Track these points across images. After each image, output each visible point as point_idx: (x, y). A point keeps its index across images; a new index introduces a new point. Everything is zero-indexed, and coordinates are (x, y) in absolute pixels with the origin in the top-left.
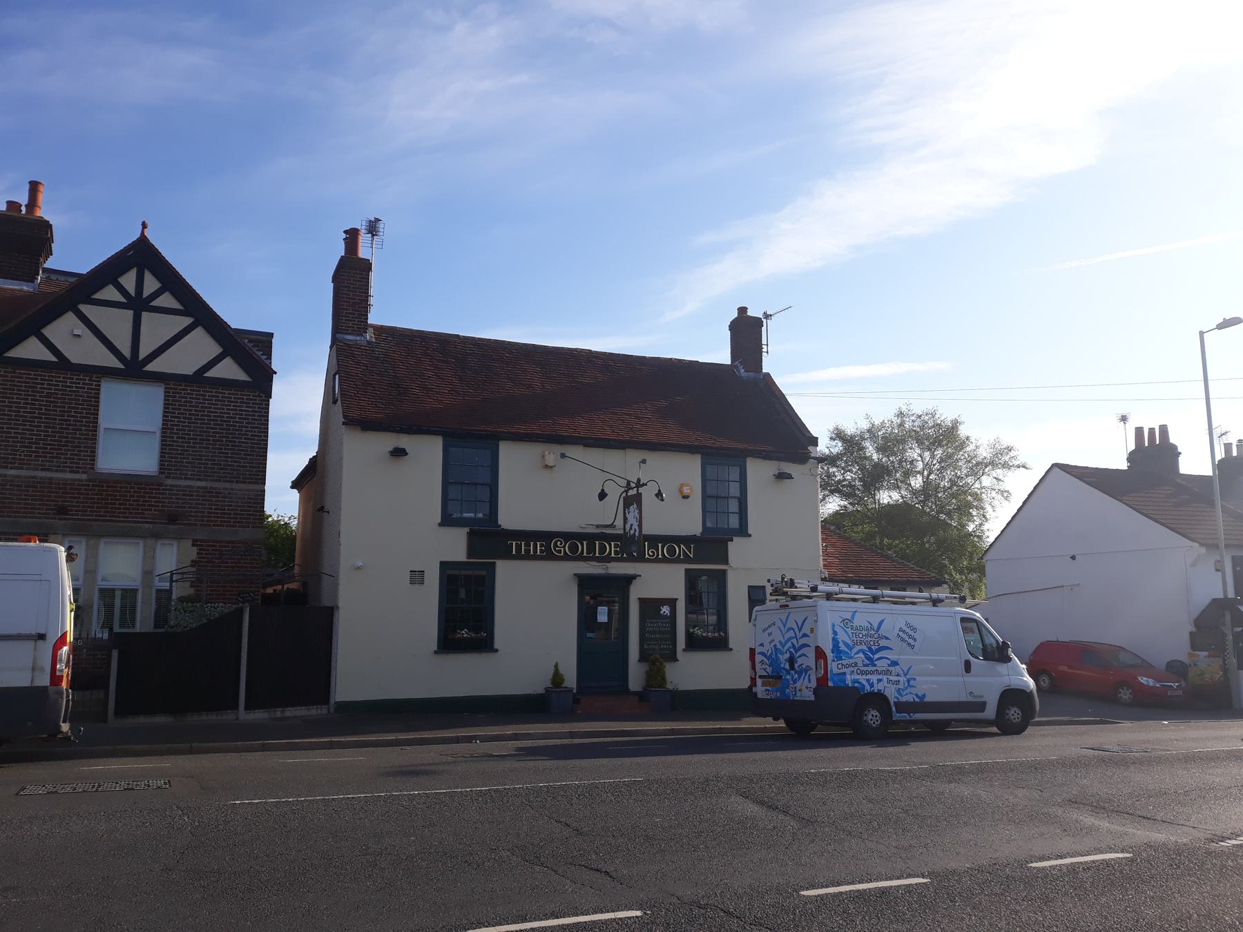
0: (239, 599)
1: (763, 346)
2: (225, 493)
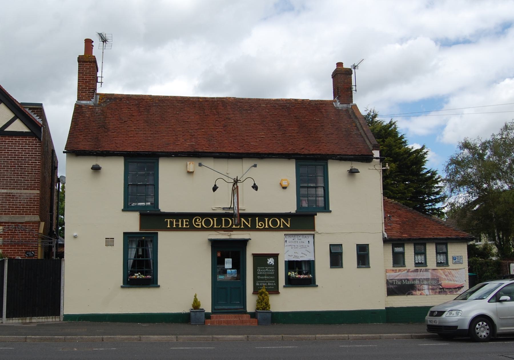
0: (26, 255)
1: (353, 87)
2: (17, 196)
